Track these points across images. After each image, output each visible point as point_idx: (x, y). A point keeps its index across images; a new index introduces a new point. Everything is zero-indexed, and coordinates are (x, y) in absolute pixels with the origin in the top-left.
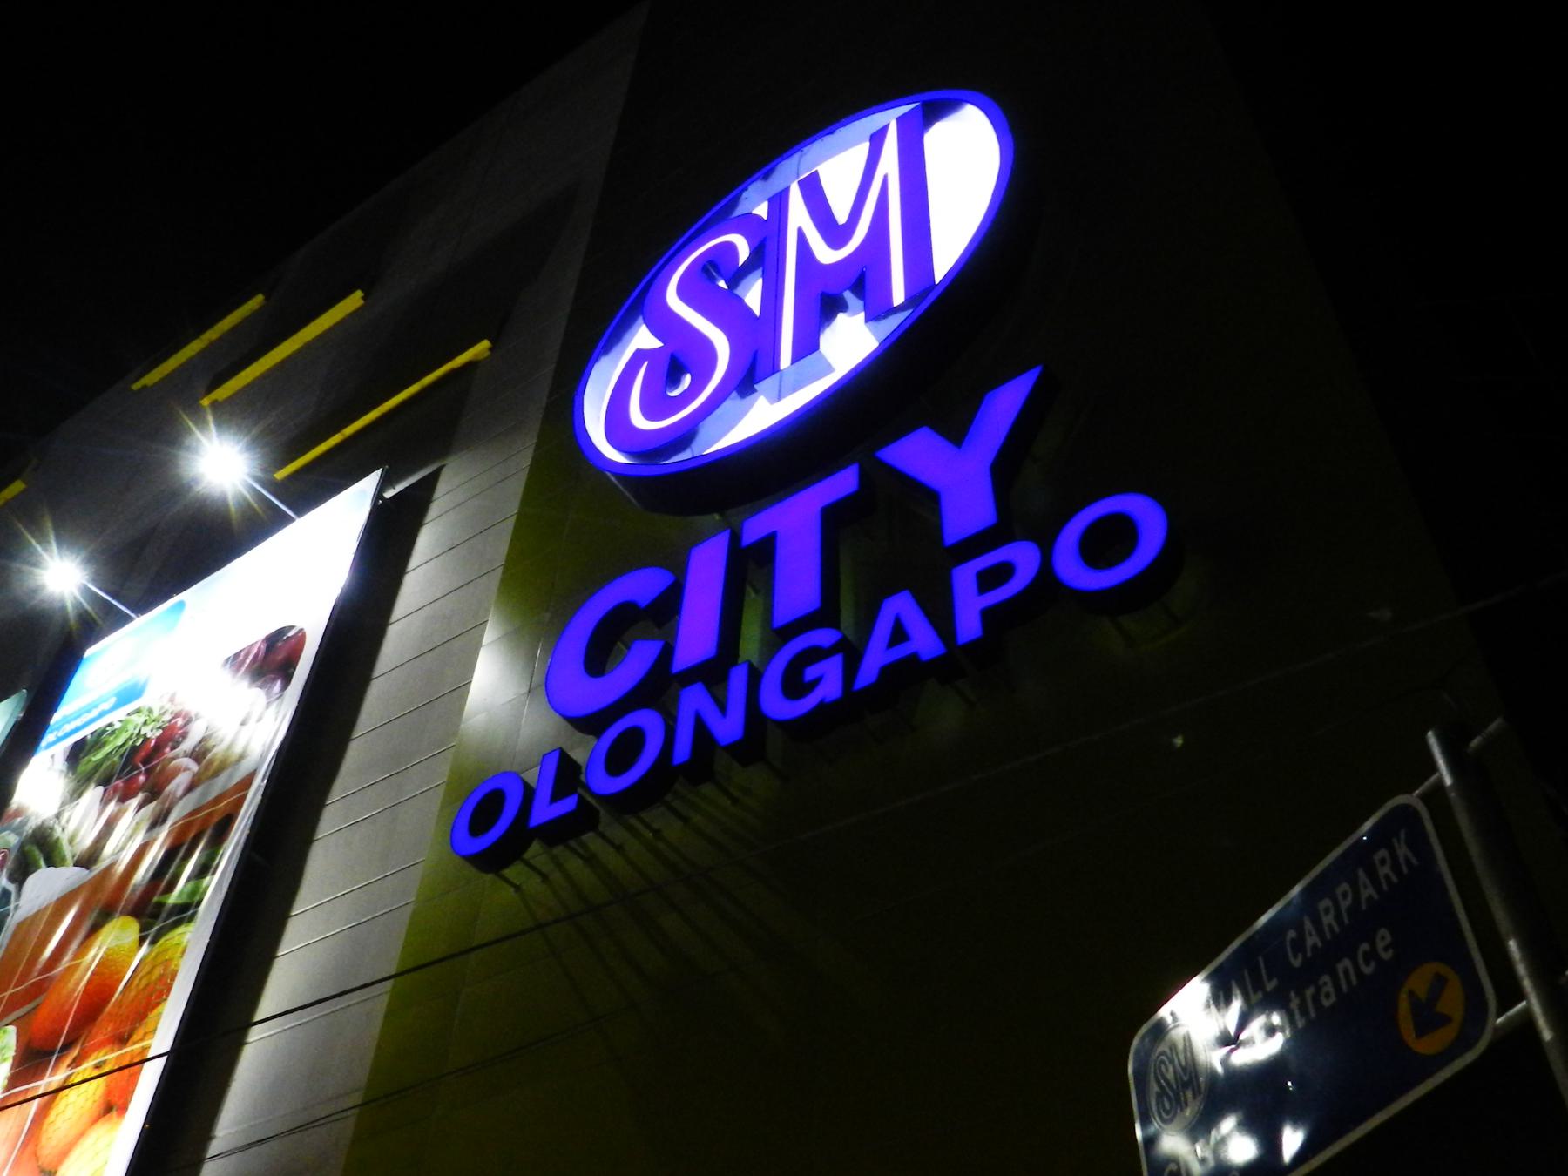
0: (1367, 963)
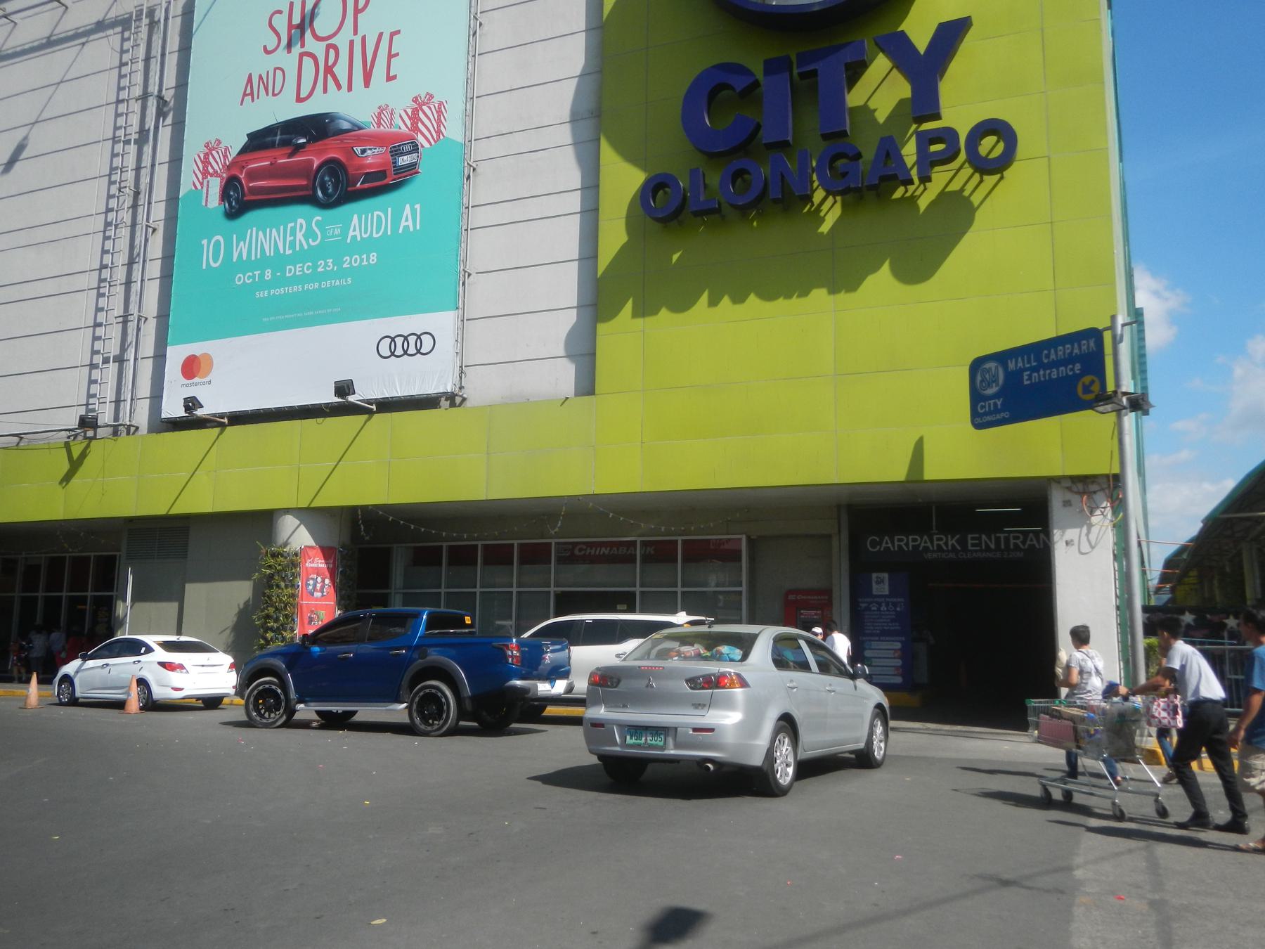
0: (1070, 371)
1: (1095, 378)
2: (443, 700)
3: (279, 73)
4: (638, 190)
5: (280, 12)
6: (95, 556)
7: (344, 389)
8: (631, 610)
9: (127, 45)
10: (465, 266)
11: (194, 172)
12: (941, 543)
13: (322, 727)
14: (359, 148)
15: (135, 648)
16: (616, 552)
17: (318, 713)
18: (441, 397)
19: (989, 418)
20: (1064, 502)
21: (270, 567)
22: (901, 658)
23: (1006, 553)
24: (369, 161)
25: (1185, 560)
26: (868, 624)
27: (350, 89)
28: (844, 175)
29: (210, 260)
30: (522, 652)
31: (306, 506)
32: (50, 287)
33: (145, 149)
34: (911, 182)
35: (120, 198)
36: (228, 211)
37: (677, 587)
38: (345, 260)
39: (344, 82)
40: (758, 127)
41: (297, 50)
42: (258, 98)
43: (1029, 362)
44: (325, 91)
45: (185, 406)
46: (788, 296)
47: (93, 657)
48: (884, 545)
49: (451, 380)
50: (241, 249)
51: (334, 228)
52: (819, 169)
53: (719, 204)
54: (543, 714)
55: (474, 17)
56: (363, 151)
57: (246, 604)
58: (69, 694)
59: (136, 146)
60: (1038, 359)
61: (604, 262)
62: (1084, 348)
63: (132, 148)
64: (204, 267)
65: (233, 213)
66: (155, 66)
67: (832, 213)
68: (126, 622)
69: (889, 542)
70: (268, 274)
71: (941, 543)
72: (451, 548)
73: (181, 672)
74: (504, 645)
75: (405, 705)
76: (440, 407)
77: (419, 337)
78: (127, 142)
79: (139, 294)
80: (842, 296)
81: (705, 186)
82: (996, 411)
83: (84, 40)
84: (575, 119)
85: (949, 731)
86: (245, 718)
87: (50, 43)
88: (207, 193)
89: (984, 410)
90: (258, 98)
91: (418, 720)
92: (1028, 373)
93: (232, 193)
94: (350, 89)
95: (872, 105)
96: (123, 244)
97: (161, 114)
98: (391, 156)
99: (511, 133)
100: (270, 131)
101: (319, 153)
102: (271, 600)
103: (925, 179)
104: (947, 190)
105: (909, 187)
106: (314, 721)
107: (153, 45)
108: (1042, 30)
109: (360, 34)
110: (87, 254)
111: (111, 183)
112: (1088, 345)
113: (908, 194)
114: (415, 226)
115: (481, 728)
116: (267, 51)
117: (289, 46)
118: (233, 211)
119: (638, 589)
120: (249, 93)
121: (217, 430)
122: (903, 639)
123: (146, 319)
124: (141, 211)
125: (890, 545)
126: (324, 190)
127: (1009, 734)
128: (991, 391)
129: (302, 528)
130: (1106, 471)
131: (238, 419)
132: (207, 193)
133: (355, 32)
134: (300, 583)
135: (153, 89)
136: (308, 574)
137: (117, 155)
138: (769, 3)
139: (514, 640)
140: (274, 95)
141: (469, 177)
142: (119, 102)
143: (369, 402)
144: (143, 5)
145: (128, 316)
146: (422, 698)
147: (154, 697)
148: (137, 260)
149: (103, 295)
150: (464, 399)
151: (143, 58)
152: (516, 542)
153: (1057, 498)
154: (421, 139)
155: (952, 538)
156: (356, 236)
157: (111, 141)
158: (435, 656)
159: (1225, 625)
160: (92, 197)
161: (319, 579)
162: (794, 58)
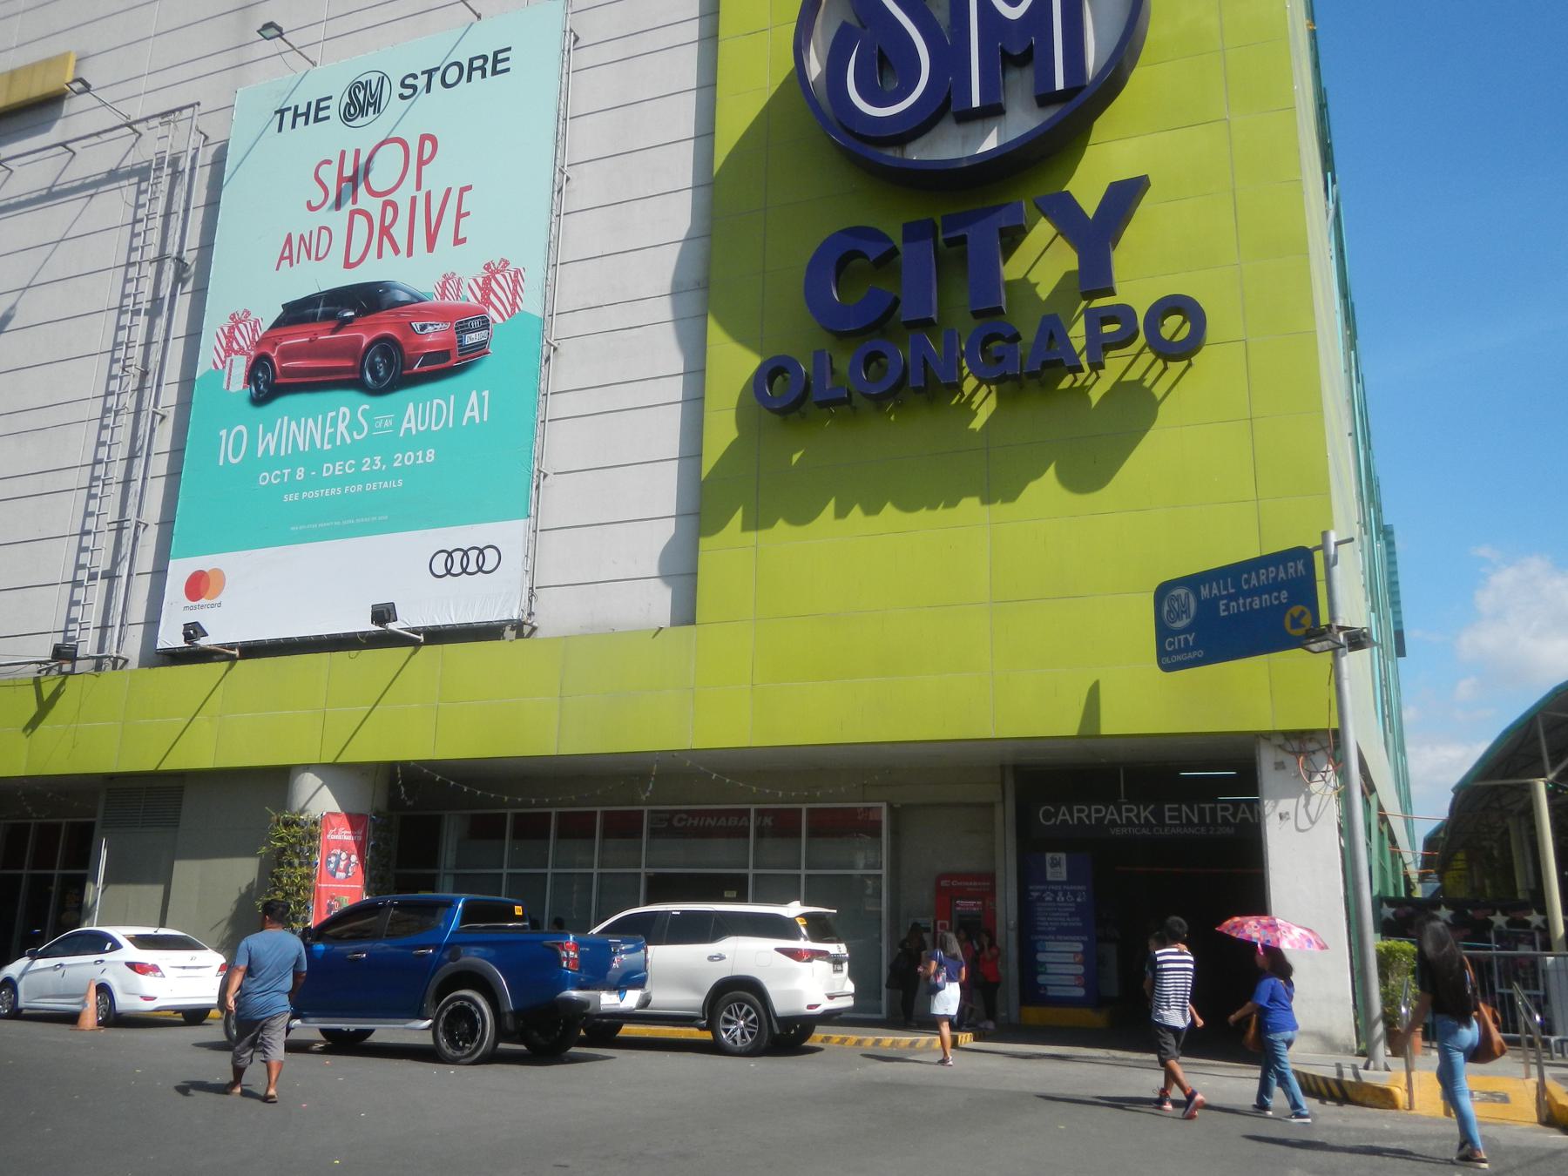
1: (1306, 609)
2: (478, 1016)
3: (325, 234)
4: (749, 379)
5: (328, 162)
6: (67, 823)
7: (382, 614)
8: (742, 899)
9: (143, 199)
10: (540, 464)
11: (215, 349)
12: (1131, 815)
13: (326, 1051)
14: (418, 324)
15: (99, 943)
16: (725, 824)
17: (323, 1031)
18: (505, 625)
19: (1179, 658)
20: (1276, 763)
21: (281, 839)
22: (1083, 963)
23: (1212, 828)
24: (430, 339)
25: (1443, 839)
26: (1042, 919)
27: (410, 253)
28: (999, 359)
29: (228, 454)
30: (581, 954)
31: (331, 761)
32: (32, 485)
33: (158, 321)
34: (1081, 369)
35: (124, 378)
36: (254, 396)
37: (800, 868)
38: (395, 457)
39: (402, 244)
40: (896, 302)
41: (348, 206)
42: (298, 262)
43: (1226, 588)
44: (380, 255)
45: (184, 634)
46: (933, 506)
47: (44, 955)
48: (1060, 817)
49: (518, 604)
50: (268, 444)
51: (385, 419)
52: (969, 355)
53: (849, 394)
54: (618, 1035)
55: (560, 170)
56: (423, 328)
57: (250, 887)
58: (10, 1003)
59: (147, 318)
60: (1237, 585)
61: (708, 464)
62: (1291, 571)
63: (142, 320)
64: (221, 464)
65: (259, 400)
66: (176, 224)
67: (985, 407)
68: (95, 910)
69: (1115, 812)
70: (300, 473)
71: (1131, 815)
72: (517, 816)
73: (155, 976)
74: (558, 944)
75: (429, 1022)
76: (504, 639)
77: (481, 551)
78: (136, 313)
79: (138, 495)
80: (999, 508)
81: (833, 372)
82: (1187, 649)
83: (92, 192)
84: (677, 291)
85: (1137, 1060)
86: (224, 1038)
87: (51, 195)
88: (230, 374)
89: (1173, 647)
90: (298, 262)
91: (444, 1042)
92: (1225, 602)
93: (260, 375)
94: (410, 253)
95: (1032, 278)
96: (123, 435)
97: (179, 279)
98: (457, 333)
99: (601, 306)
100: (310, 301)
101: (368, 329)
102: (280, 882)
103: (1097, 366)
104: (1124, 379)
105: (1078, 375)
106: (319, 1042)
107: (175, 199)
108: (1234, 190)
109: (424, 189)
110: (80, 445)
111: (114, 361)
112: (1296, 568)
113: (1077, 384)
114: (481, 414)
115: (530, 1053)
116: (311, 208)
117: (338, 205)
118: (261, 395)
119: (751, 872)
120: (287, 256)
121: (225, 665)
122: (1085, 938)
123: (147, 526)
124: (149, 395)
125: (1068, 817)
126: (374, 374)
127: (1214, 1065)
128: (1180, 624)
129: (325, 788)
130: (1323, 725)
131: (253, 650)
132: (230, 374)
133: (419, 187)
134: (319, 861)
135: (172, 250)
136: (330, 849)
137: (123, 328)
138: (909, 158)
139: (571, 938)
140: (317, 259)
141: (548, 359)
142: (129, 264)
143: (415, 631)
144: (165, 152)
145: (123, 521)
146: (450, 1014)
147: (117, 1009)
148: (139, 454)
149: (95, 496)
150: (534, 629)
151: (163, 213)
152: (599, 810)
153: (1267, 759)
154: (492, 313)
155: (1145, 810)
156: (474, 417)
157: (117, 311)
158: (472, 957)
159: (1492, 923)
160: (90, 377)
161: (344, 856)
162: (939, 222)
